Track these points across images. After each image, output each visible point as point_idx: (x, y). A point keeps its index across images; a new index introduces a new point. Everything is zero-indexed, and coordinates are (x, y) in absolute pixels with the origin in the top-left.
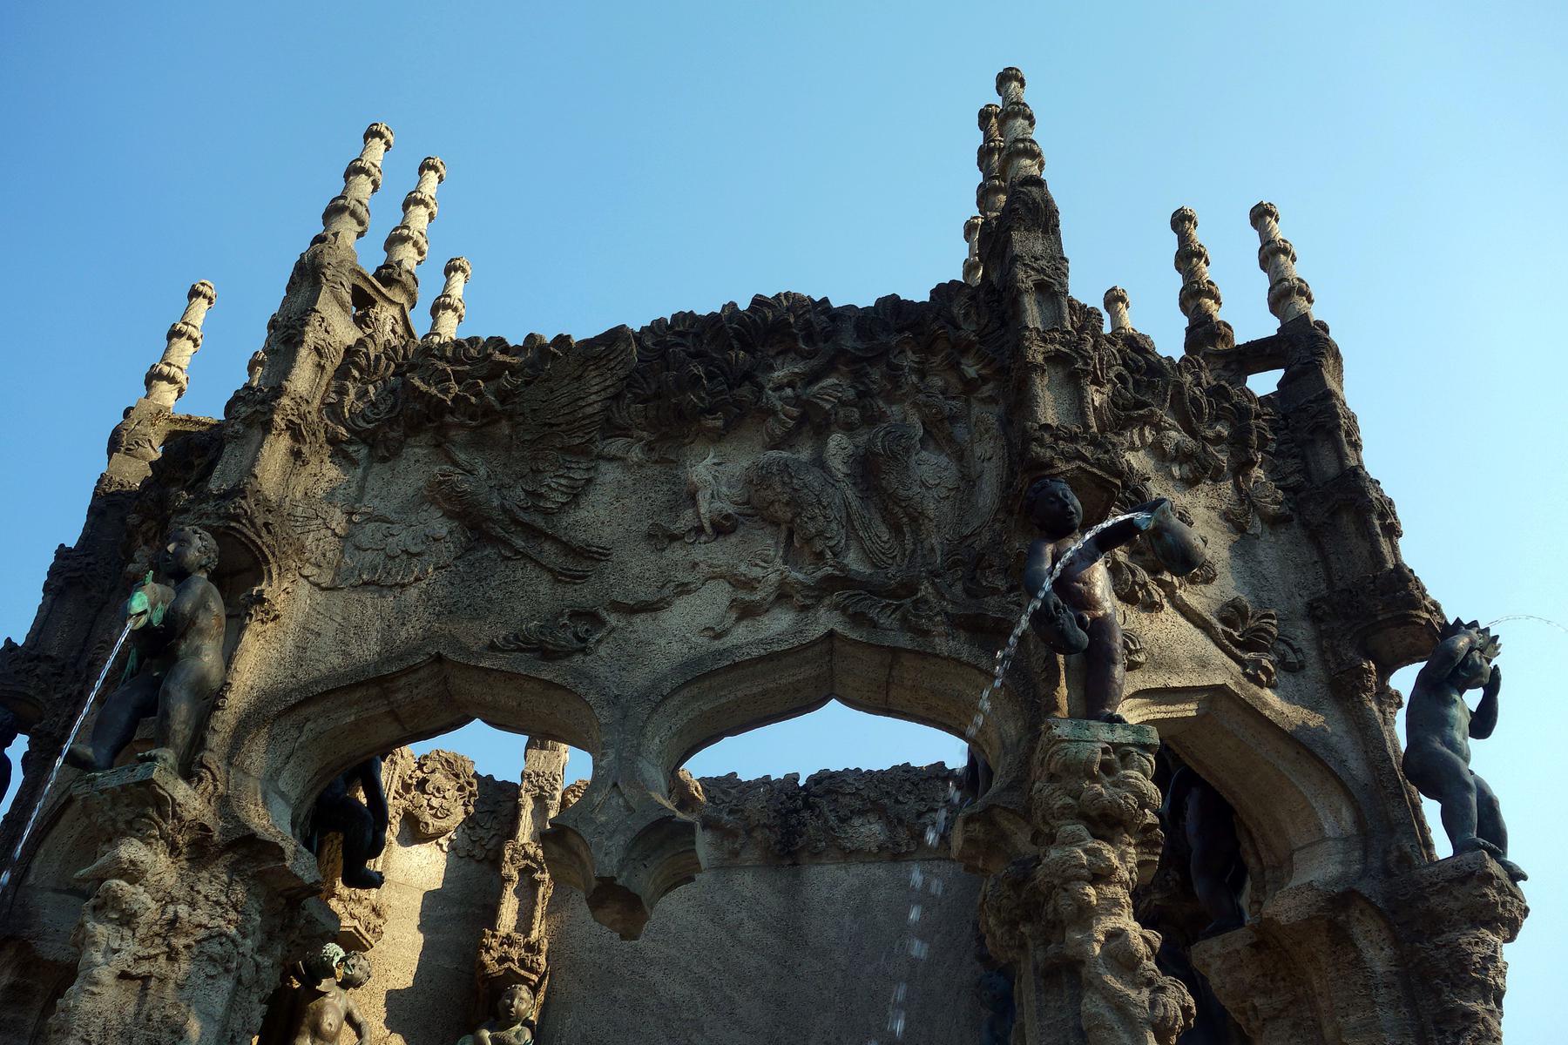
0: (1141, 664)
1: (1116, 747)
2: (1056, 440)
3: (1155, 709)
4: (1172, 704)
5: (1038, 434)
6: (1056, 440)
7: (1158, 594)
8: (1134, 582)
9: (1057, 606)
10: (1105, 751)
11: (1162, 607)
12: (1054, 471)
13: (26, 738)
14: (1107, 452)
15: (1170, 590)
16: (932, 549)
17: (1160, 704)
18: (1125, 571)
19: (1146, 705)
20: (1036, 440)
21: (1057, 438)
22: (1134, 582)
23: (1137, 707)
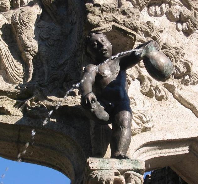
0: (150, 129)
1: (123, 172)
2: (102, 12)
3: (159, 151)
4: (168, 148)
5: (92, 9)
6: (102, 12)
7: (164, 91)
8: (151, 86)
9: (93, 99)
10: (116, 174)
11: (167, 99)
12: (100, 28)
13: (187, 152)
14: (129, 17)
15: (171, 88)
16: (44, 73)
17: (161, 149)
18: (146, 80)
19: (154, 149)
20: (91, 12)
21: (102, 11)
22: (151, 86)
23: (148, 151)
